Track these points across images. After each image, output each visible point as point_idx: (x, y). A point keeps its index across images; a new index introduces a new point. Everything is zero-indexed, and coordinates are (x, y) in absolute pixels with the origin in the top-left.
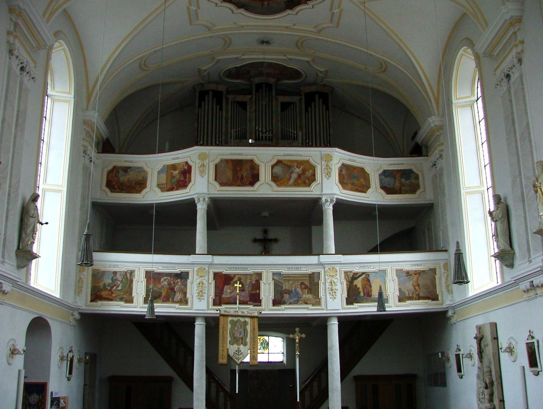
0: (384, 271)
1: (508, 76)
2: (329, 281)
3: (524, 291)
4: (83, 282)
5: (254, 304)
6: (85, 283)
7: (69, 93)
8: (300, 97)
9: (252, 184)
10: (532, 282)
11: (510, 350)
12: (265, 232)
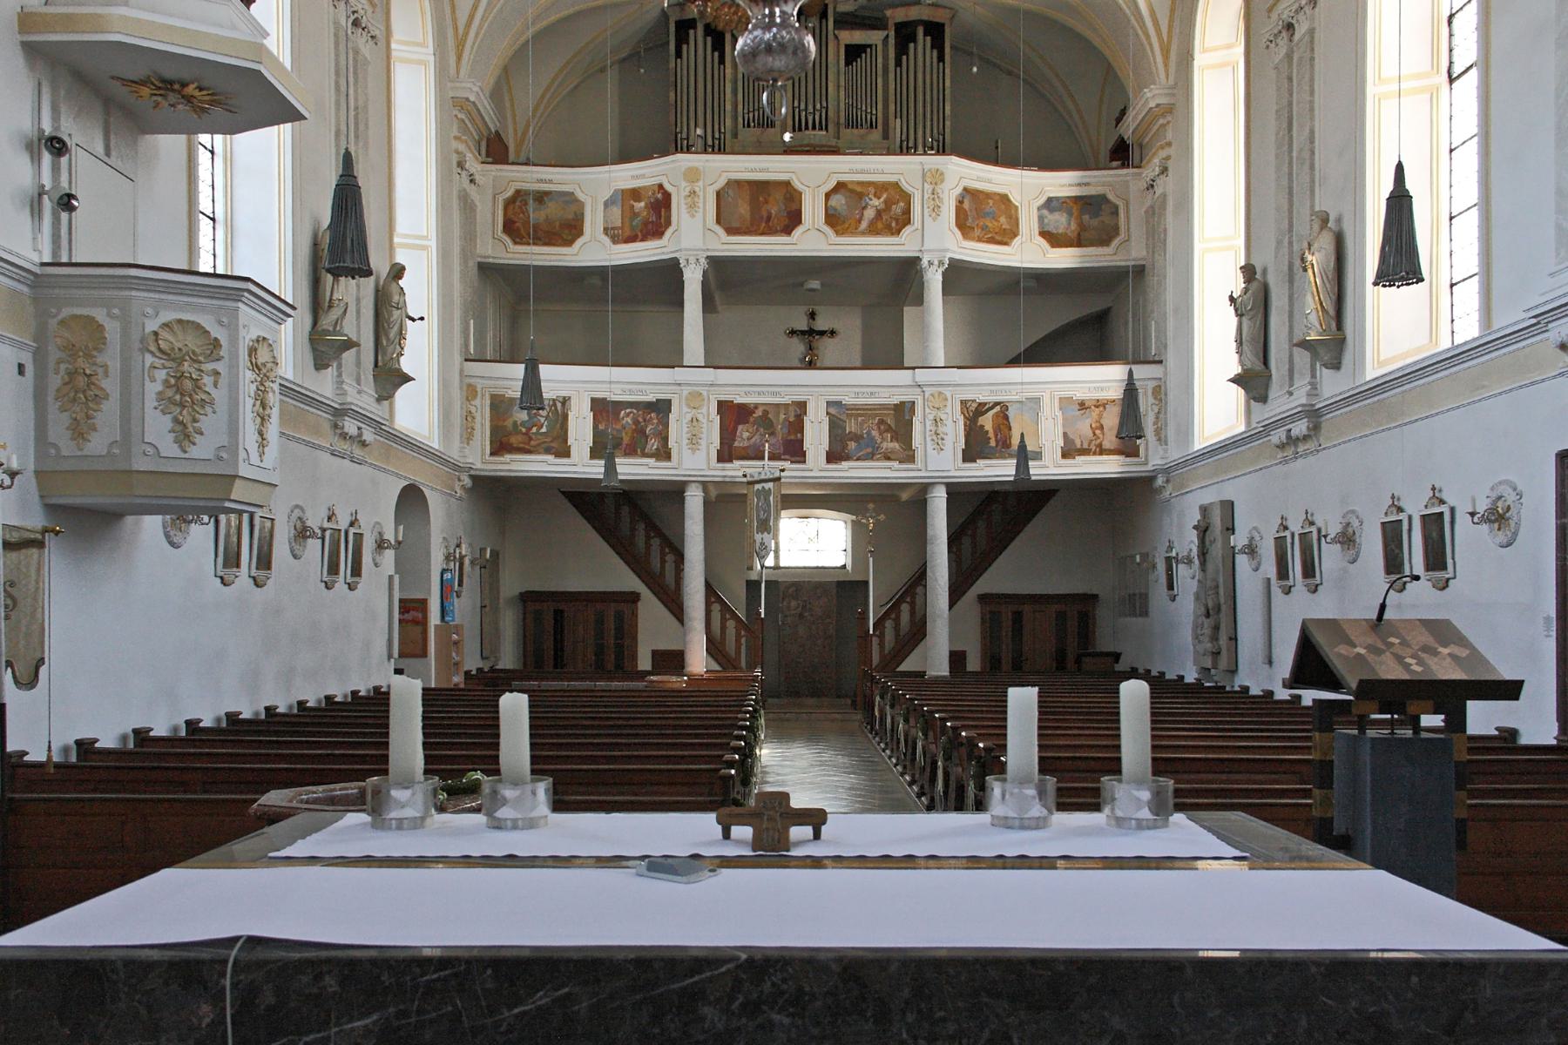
0: (1037, 401)
1: (1290, 27)
2: (931, 417)
3: (1278, 447)
4: (474, 418)
5: (793, 459)
6: (478, 419)
7: (423, 45)
8: (886, 33)
9: (788, 230)
10: (1290, 430)
11: (1251, 550)
12: (812, 315)
